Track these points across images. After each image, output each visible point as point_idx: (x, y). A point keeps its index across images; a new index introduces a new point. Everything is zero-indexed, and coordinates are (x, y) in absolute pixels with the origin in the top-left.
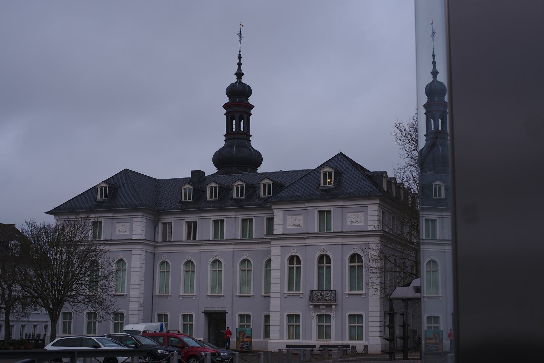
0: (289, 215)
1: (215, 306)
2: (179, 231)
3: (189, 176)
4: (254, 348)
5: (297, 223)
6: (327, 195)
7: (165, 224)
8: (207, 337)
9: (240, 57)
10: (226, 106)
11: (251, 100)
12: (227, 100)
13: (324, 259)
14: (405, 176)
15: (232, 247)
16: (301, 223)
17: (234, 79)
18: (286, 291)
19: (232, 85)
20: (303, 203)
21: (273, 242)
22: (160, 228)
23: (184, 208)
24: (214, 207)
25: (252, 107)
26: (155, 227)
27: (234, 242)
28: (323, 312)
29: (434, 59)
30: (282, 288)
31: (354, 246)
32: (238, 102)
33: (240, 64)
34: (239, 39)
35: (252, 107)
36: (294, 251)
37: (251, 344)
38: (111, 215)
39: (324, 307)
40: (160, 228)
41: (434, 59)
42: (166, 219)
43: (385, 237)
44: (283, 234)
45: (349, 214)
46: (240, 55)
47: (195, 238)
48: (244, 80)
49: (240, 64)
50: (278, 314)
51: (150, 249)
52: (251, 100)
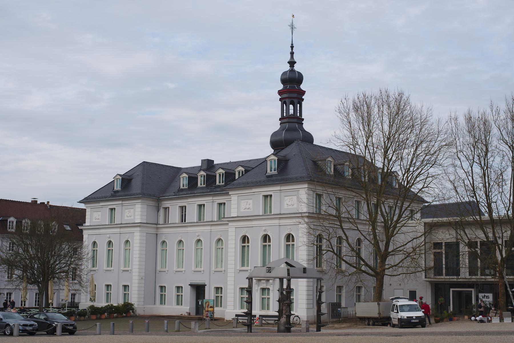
0: (242, 200)
1: (198, 280)
2: (175, 216)
3: (199, 164)
4: (216, 316)
5: (248, 207)
6: (270, 181)
7: (166, 208)
8: (194, 306)
9: (292, 47)
10: (280, 93)
11: (303, 87)
12: (281, 87)
13: (266, 238)
15: (209, 228)
16: (251, 206)
18: (239, 267)
19: (284, 74)
20: (251, 189)
21: (230, 224)
22: (162, 211)
23: (180, 194)
24: (203, 194)
25: (303, 93)
26: (158, 212)
27: (211, 223)
28: (264, 286)
29: (292, 49)
30: (235, 264)
31: (289, 226)
32: (292, 88)
33: (292, 53)
34: (291, 30)
35: (303, 93)
37: (213, 313)
38: (120, 202)
39: (264, 281)
40: (162, 211)
41: (292, 49)
42: (166, 204)
43: (315, 217)
44: (90, 226)
46: (292, 44)
47: (185, 221)
48: (297, 68)
49: (292, 53)
50: (233, 287)
51: (153, 231)
52: (303, 87)
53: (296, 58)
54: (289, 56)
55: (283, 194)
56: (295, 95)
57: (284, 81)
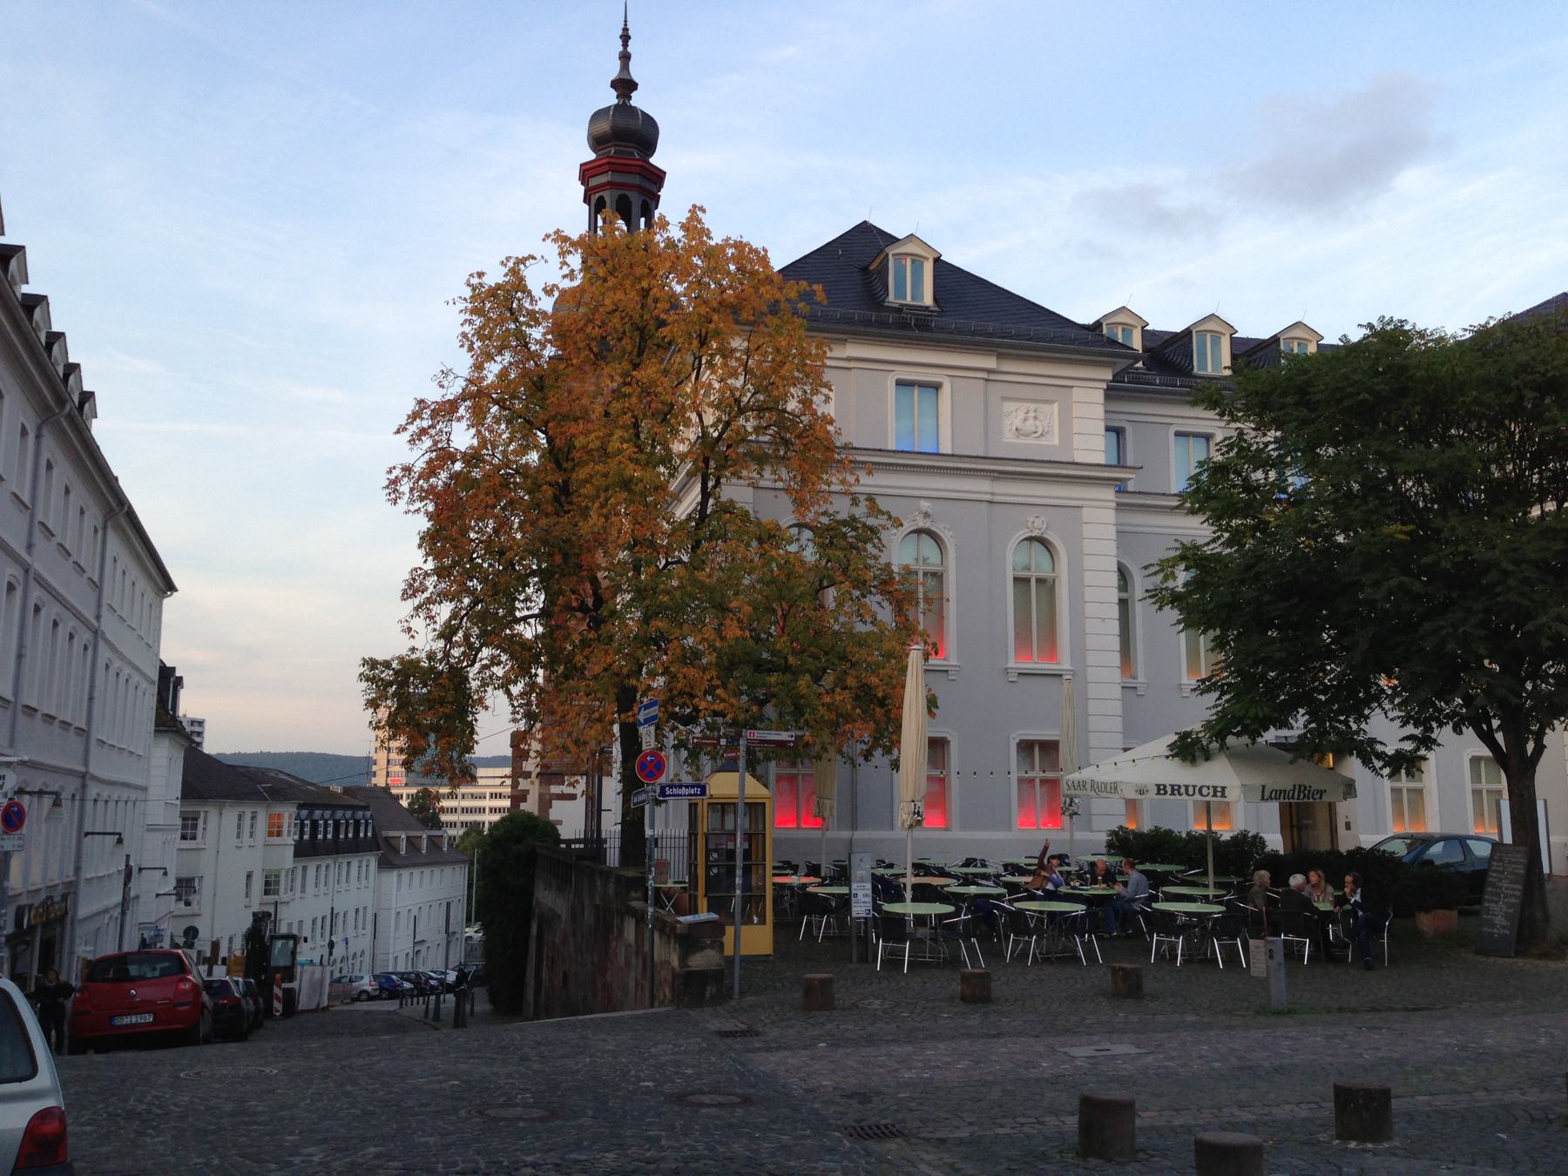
9: (625, 38)
14: (876, 657)
17: (610, 98)
19: (598, 116)
29: (625, 45)
33: (625, 57)
36: (1038, 523)
38: (990, 362)
41: (625, 45)
45: (1009, 406)
46: (626, 29)
48: (637, 100)
49: (625, 57)
53: (635, 72)
54: (617, 64)
55: (996, 390)
56: (636, 180)
57: (597, 142)
